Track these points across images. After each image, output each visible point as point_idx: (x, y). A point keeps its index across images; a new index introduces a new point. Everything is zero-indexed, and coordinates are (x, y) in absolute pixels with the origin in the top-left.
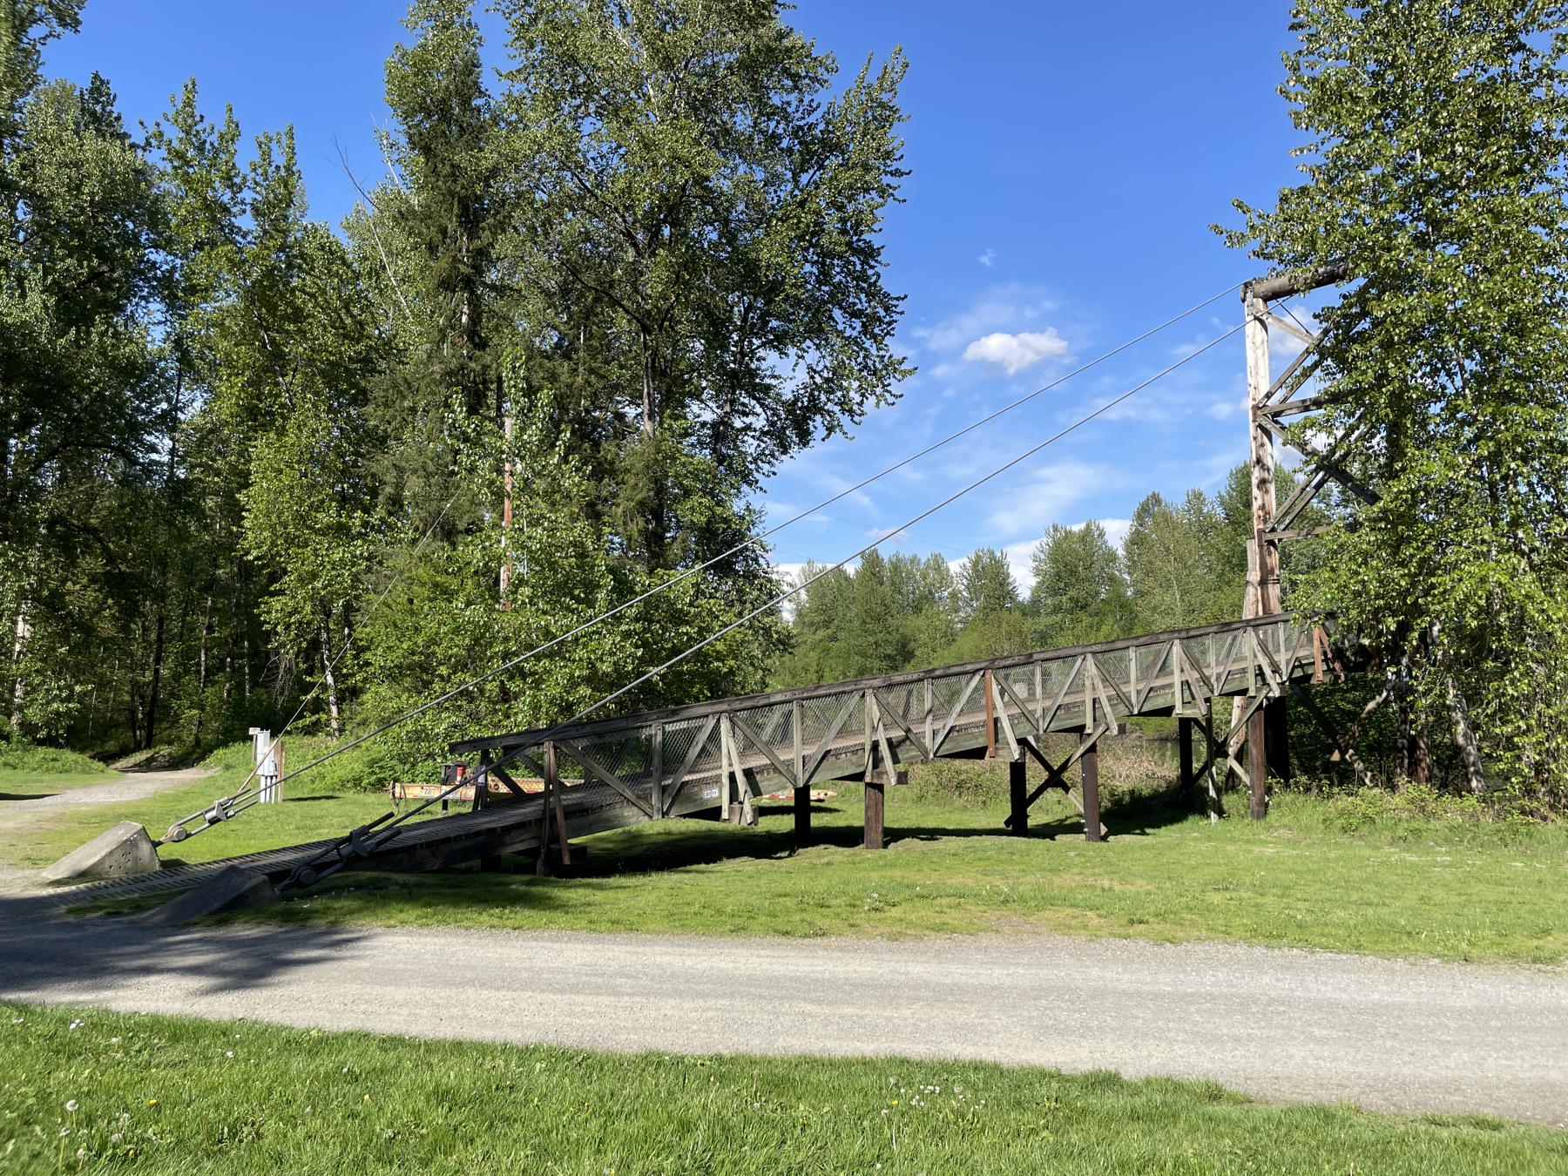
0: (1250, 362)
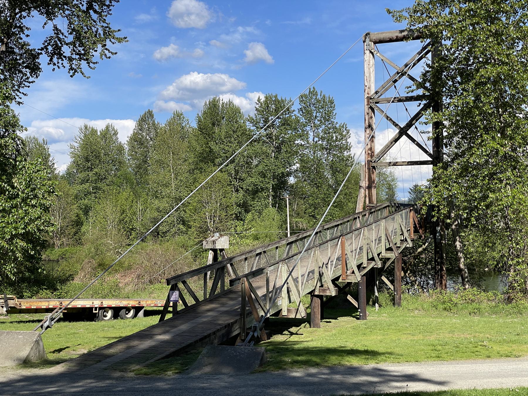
0: (367, 74)
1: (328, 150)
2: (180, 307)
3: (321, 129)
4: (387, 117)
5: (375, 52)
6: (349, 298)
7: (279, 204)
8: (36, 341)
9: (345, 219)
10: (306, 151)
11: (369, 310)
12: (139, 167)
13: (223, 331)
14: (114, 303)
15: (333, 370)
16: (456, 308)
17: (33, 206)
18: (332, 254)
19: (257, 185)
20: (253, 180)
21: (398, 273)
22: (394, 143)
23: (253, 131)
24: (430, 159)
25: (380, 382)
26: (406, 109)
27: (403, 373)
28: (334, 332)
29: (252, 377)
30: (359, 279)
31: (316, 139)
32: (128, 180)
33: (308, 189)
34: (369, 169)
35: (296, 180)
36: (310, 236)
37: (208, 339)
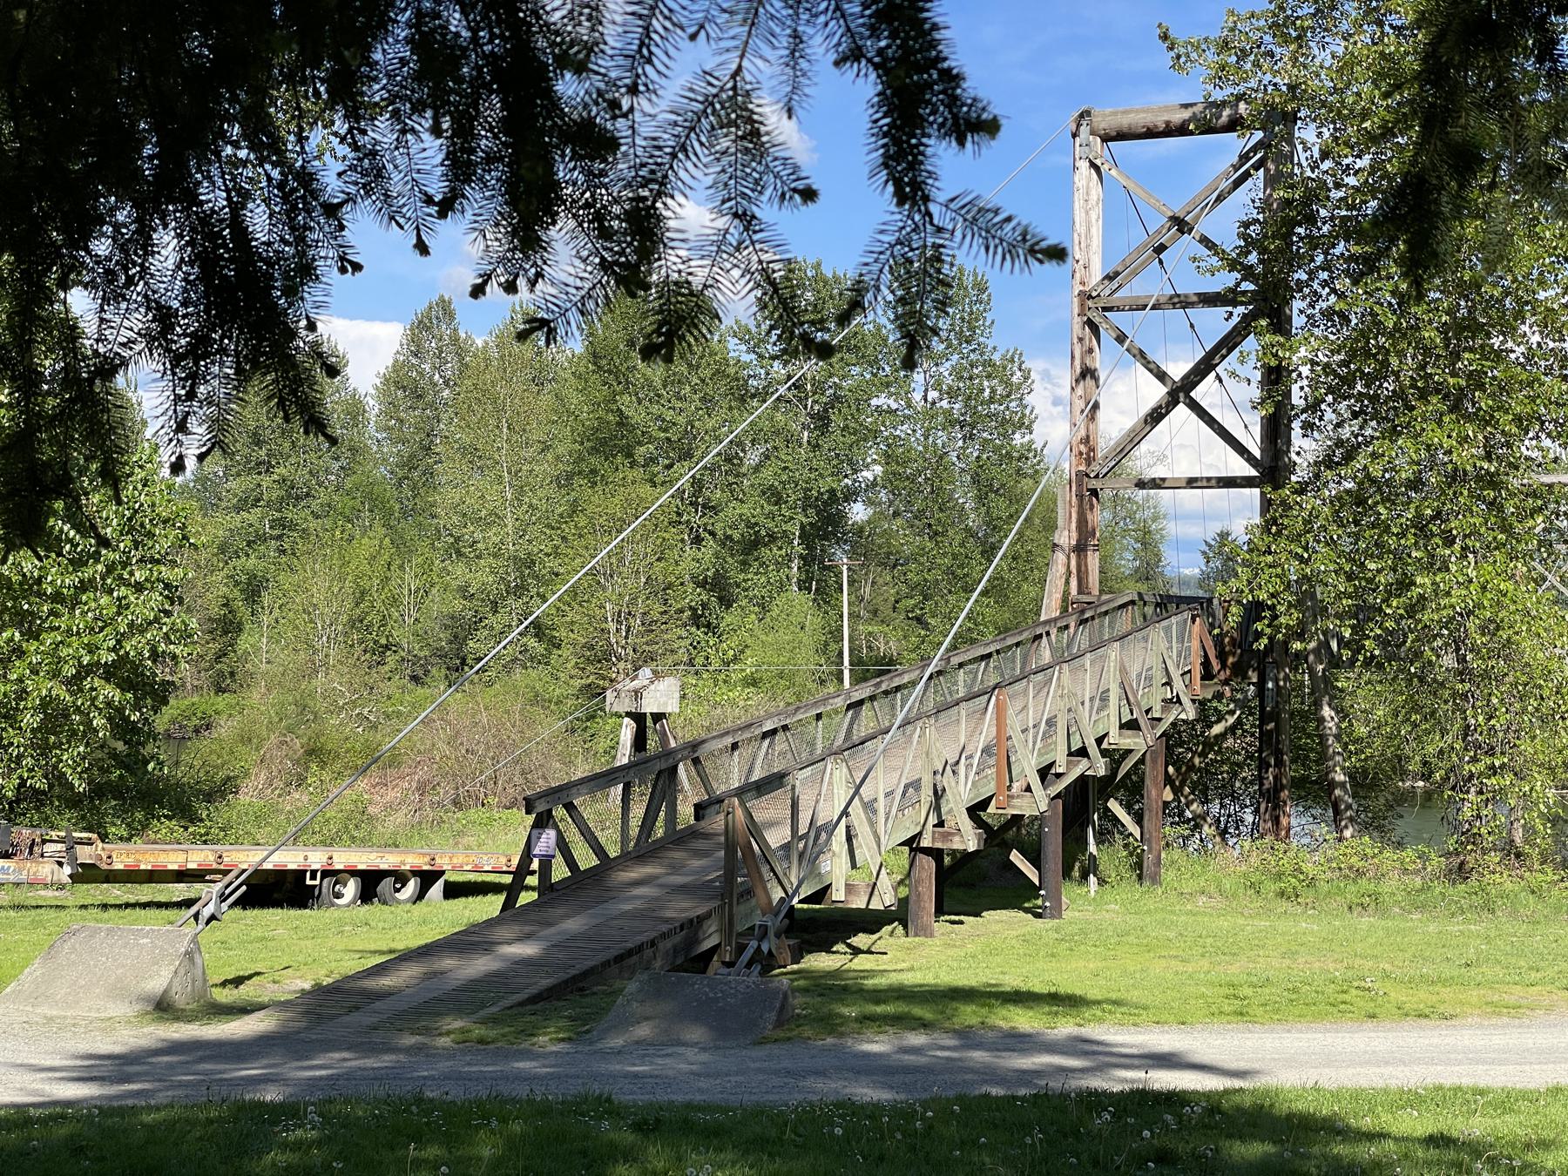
1: (968, 427)
2: (560, 872)
3: (948, 365)
5: (1106, 167)
6: (1016, 857)
7: (818, 580)
8: (187, 953)
9: (1012, 637)
11: (1070, 893)
12: (410, 464)
13: (677, 939)
14: (364, 859)
15: (968, 1038)
16: (1312, 892)
17: (139, 588)
18: (970, 736)
19: (756, 524)
20: (745, 510)
21: (1154, 793)
23: (747, 366)
24: (1254, 473)
25: (1083, 1070)
26: (1192, 326)
27: (1146, 1051)
28: (970, 948)
29: (758, 1052)
30: (1043, 808)
31: (933, 395)
32: (376, 502)
33: (905, 539)
34: (1080, 497)
35: (870, 511)
36: (914, 683)
37: (635, 959)
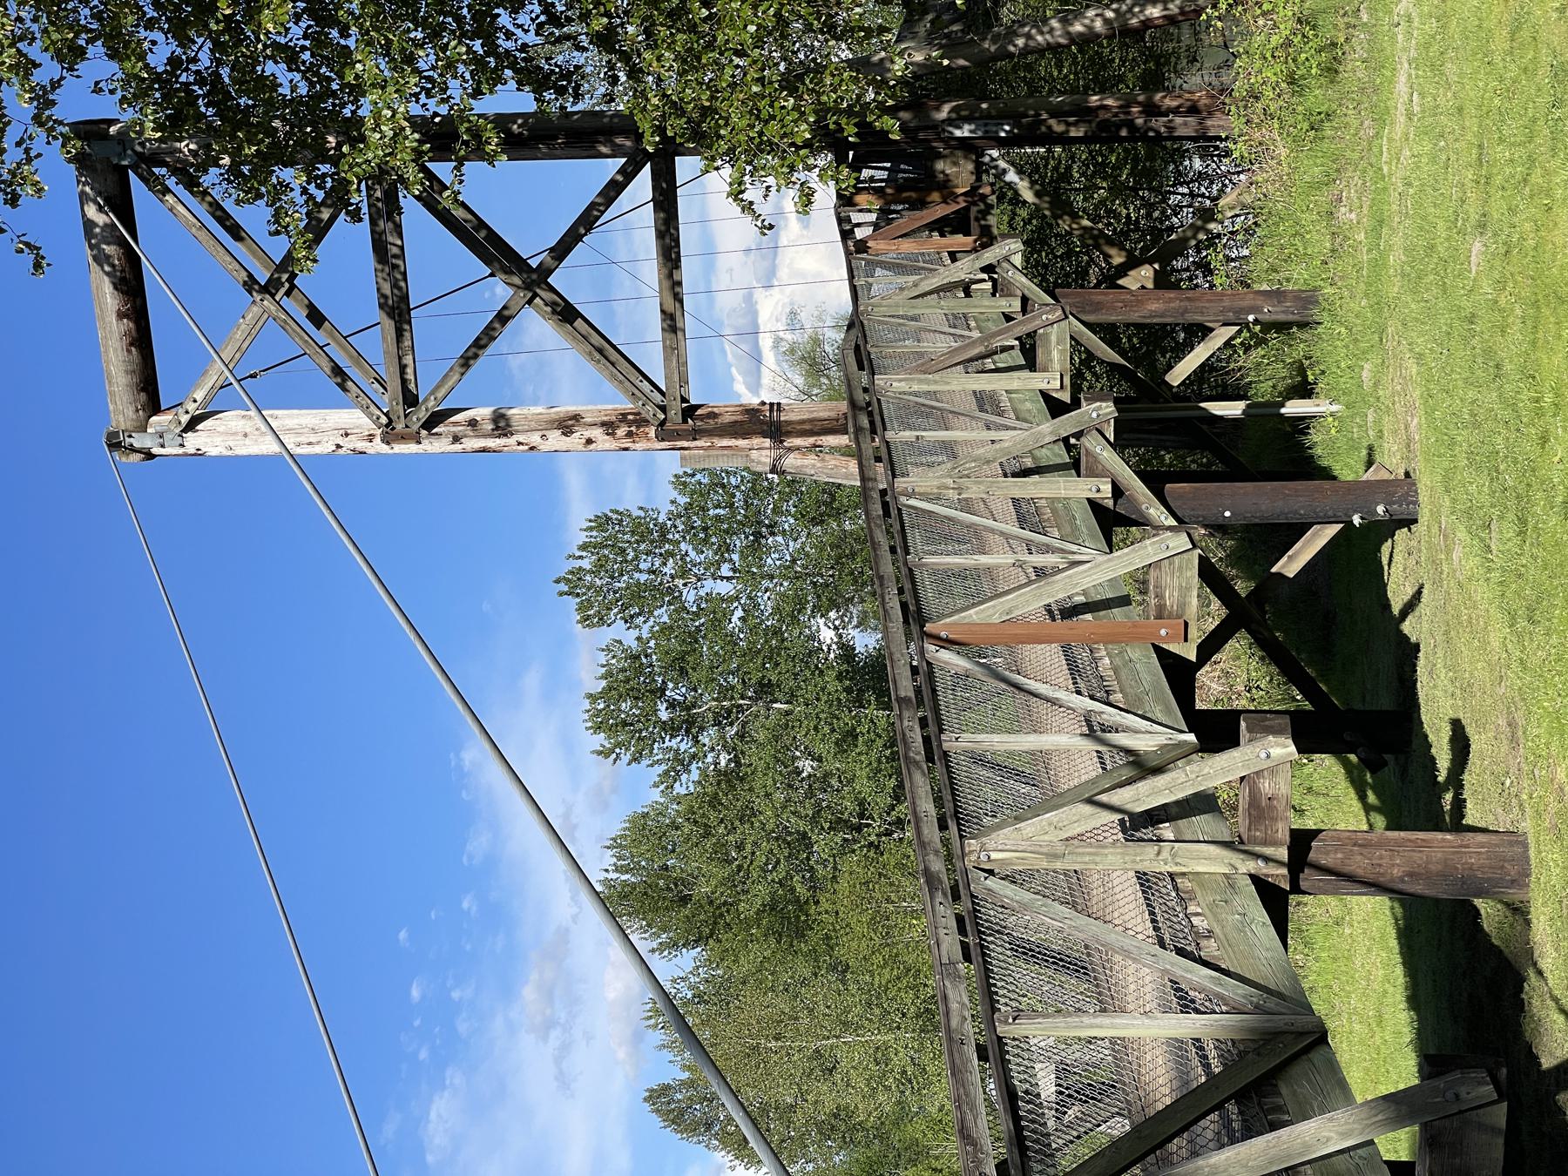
1: (759, 531)
4: (466, 361)
6: (1291, 564)
10: (766, 602)
22: (579, 323)
23: (703, 772)
31: (725, 570)
34: (695, 434)
